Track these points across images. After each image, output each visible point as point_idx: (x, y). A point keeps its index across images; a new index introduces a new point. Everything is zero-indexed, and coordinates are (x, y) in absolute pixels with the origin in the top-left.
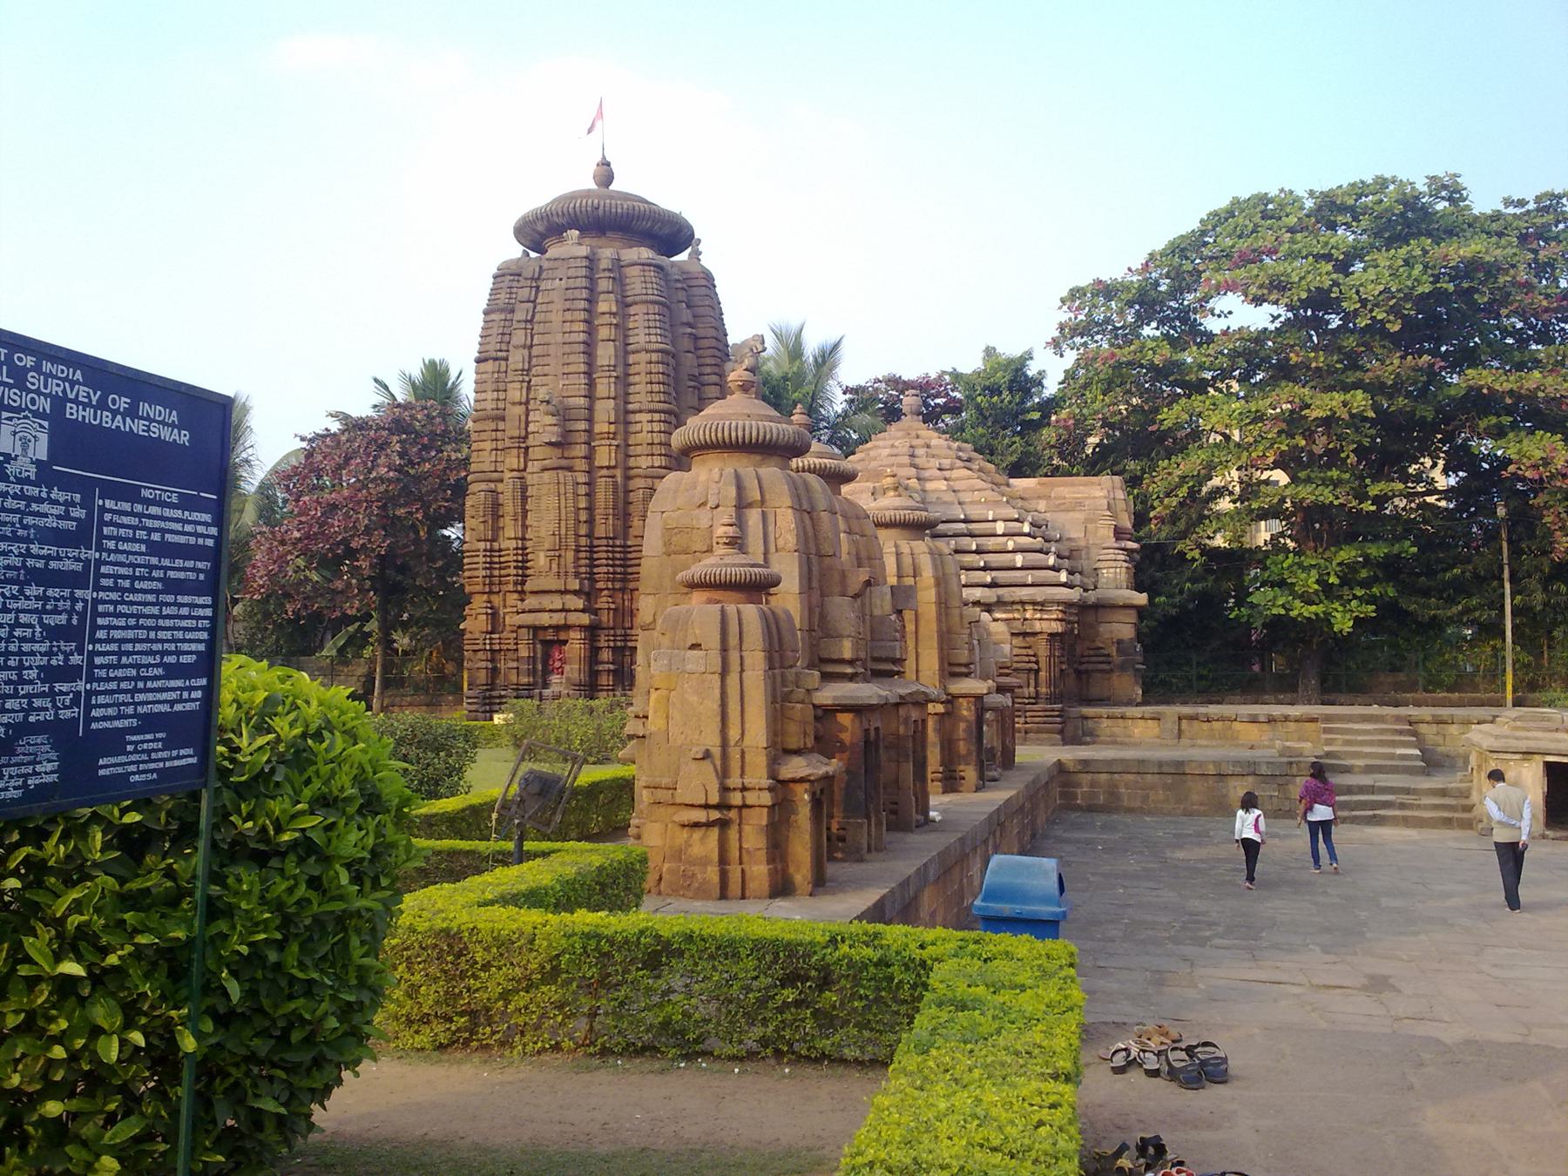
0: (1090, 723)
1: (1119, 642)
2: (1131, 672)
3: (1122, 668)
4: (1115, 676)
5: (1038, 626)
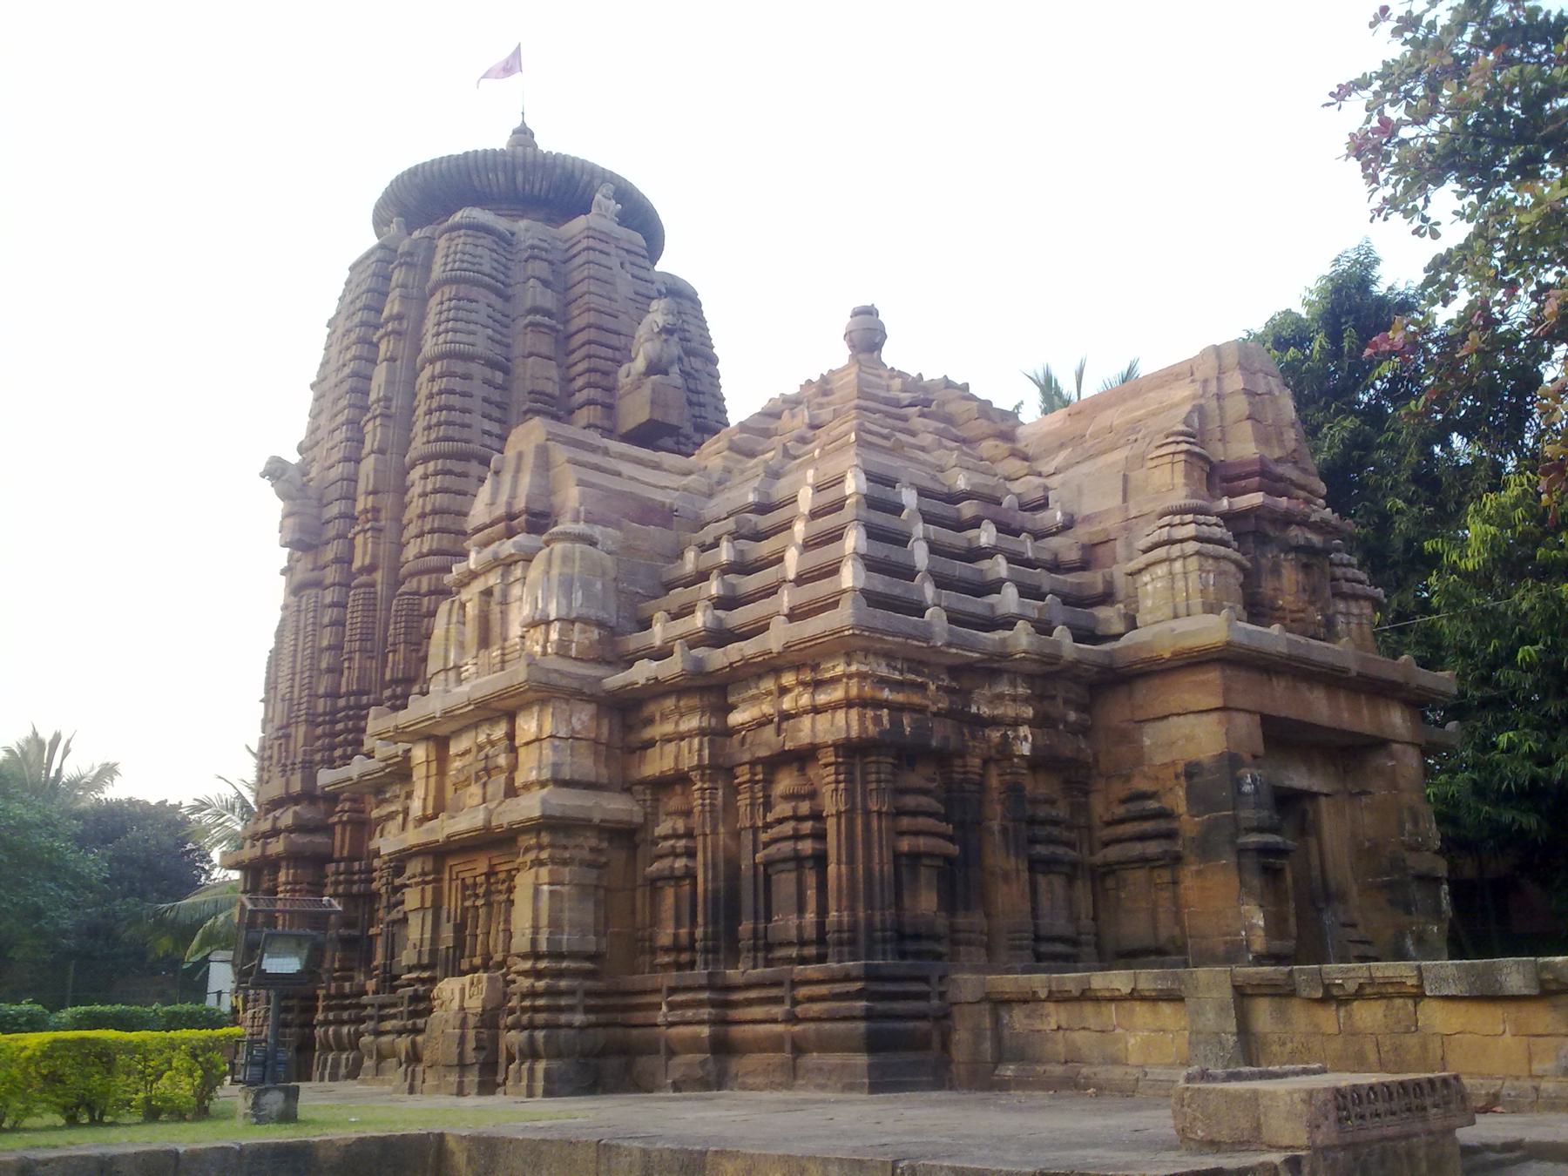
0: (1017, 1020)
1: (1192, 771)
2: (1227, 860)
3: (1205, 848)
4: (1188, 876)
5: (806, 731)
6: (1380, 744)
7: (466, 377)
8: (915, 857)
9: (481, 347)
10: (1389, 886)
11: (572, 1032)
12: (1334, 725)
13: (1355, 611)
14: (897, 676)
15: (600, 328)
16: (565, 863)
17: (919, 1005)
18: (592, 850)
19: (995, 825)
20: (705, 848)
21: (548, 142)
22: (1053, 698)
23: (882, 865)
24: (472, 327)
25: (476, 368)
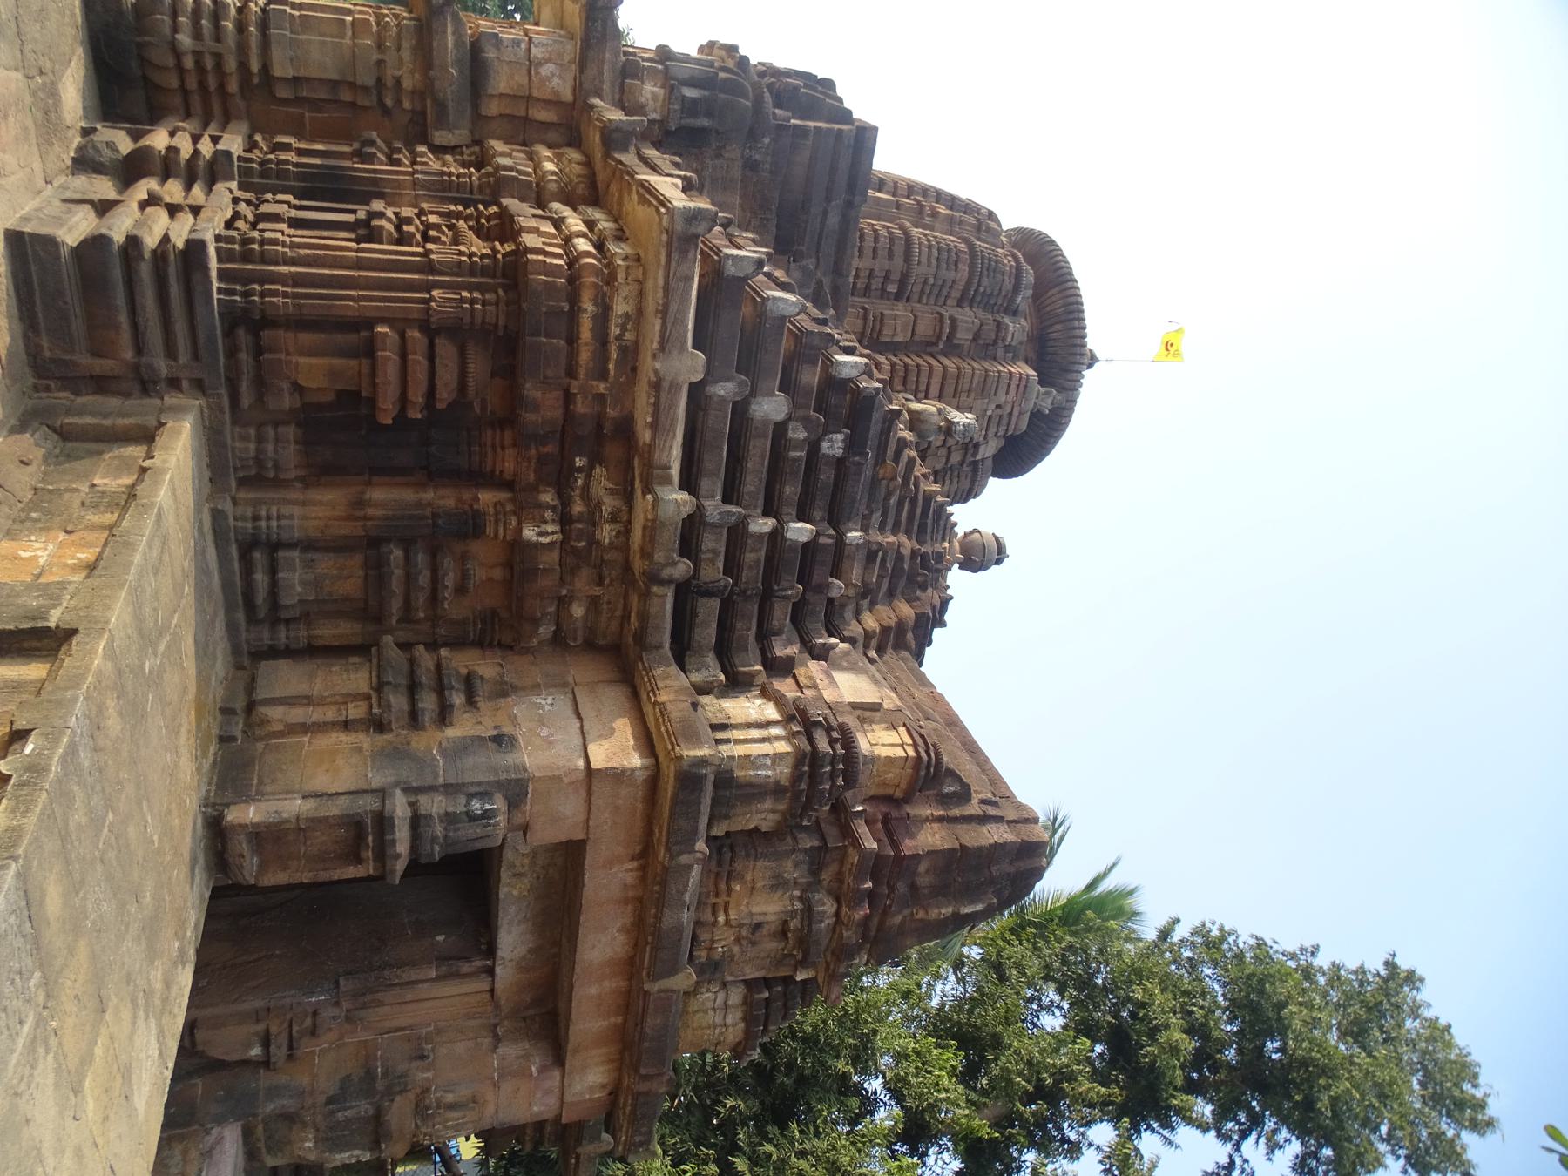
6: (558, 1053)
7: (890, 255)
8: (369, 350)
9: (918, 270)
10: (370, 1075)
11: (167, 31)
12: (578, 970)
13: (729, 1021)
14: (615, 330)
15: (944, 378)
16: (380, 46)
17: (154, 335)
18: (398, 81)
19: (429, 495)
20: (397, 173)
21: (1090, 378)
22: (600, 582)
23: (352, 303)
24: (934, 262)
25: (899, 261)
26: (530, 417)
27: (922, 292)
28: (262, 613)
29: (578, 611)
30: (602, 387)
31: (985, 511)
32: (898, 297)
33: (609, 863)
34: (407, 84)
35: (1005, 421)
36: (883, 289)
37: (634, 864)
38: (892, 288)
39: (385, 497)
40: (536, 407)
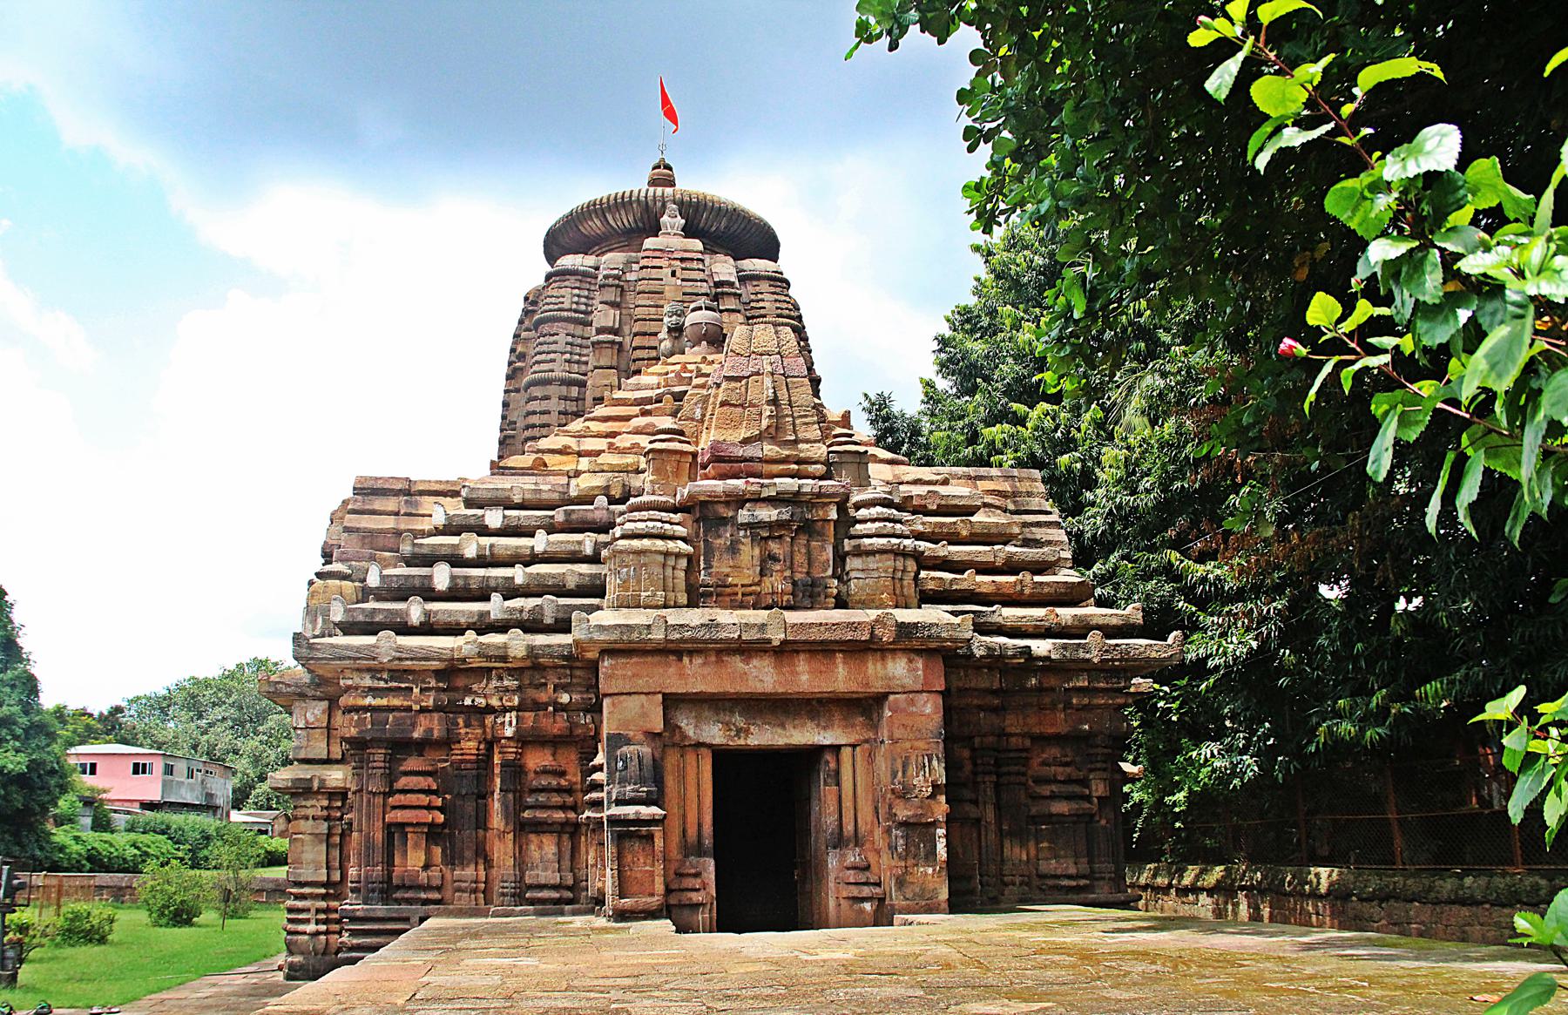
14: (382, 684)
24: (552, 356)
26: (436, 734)
27: (578, 362)
28: (569, 895)
29: (565, 698)
30: (416, 691)
31: (978, 164)
32: (583, 385)
33: (682, 675)
34: (325, 803)
35: (688, 265)
36: (577, 400)
37: (686, 660)
38: (574, 392)
39: (497, 821)
40: (430, 730)
